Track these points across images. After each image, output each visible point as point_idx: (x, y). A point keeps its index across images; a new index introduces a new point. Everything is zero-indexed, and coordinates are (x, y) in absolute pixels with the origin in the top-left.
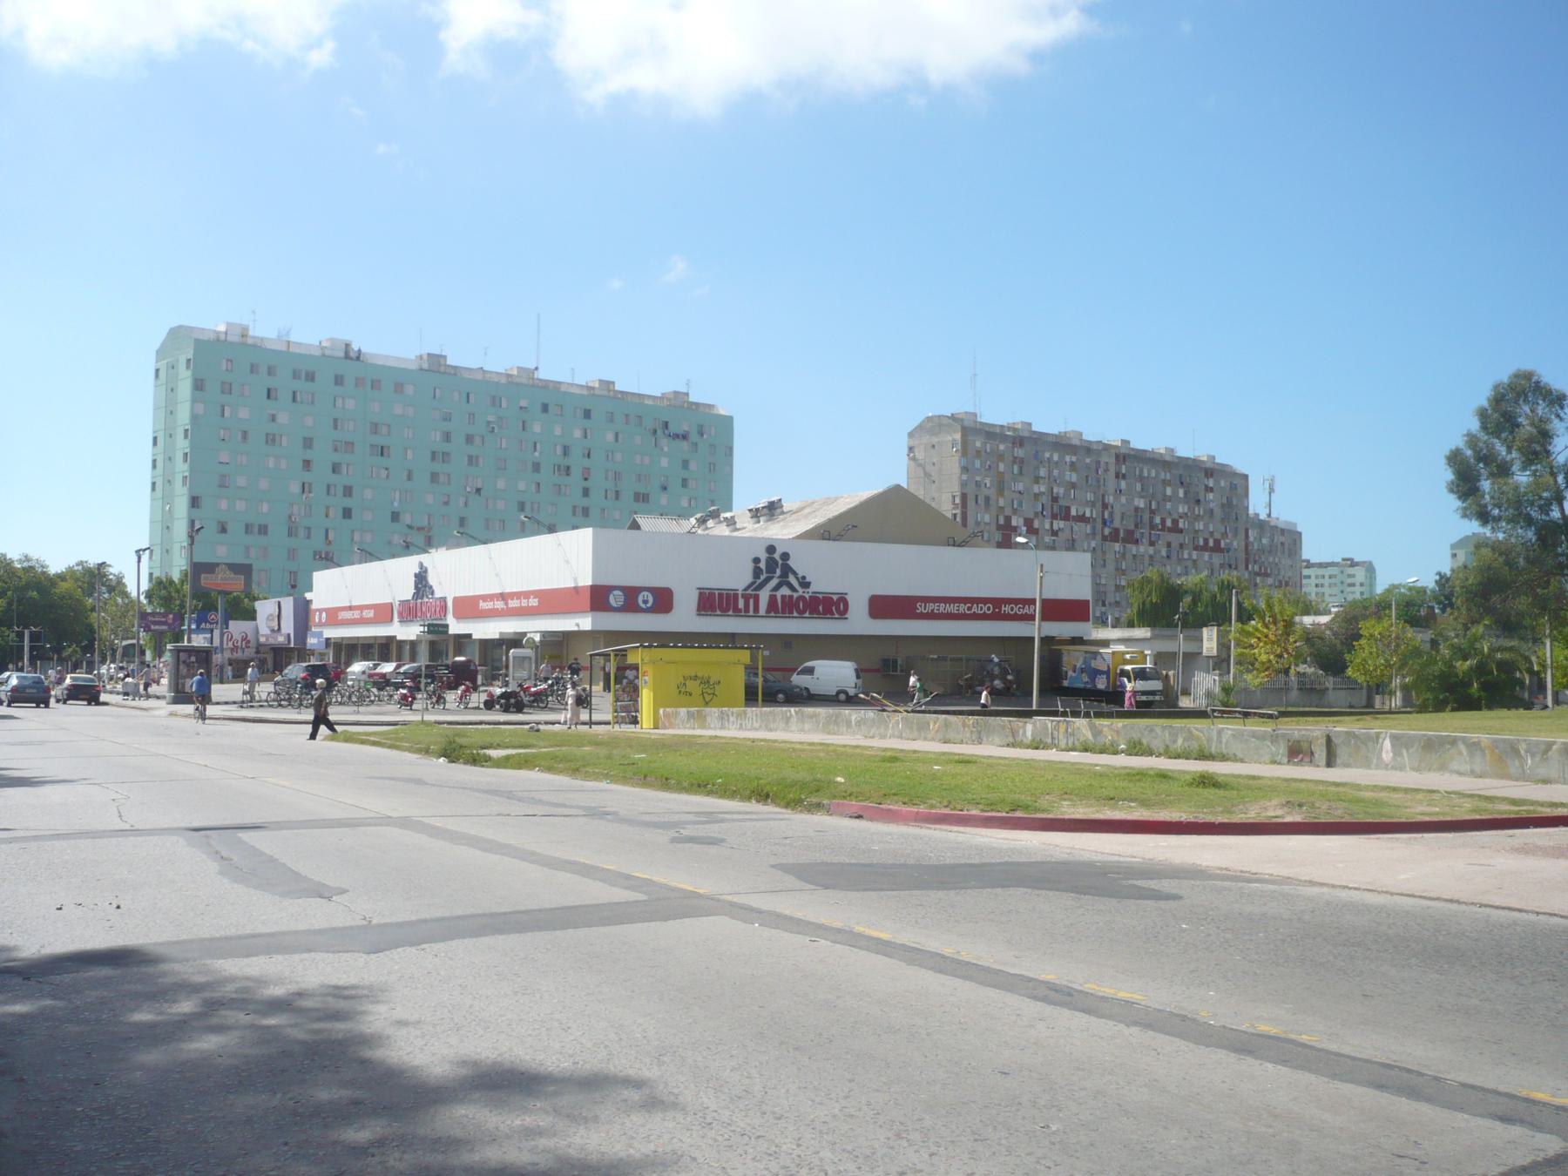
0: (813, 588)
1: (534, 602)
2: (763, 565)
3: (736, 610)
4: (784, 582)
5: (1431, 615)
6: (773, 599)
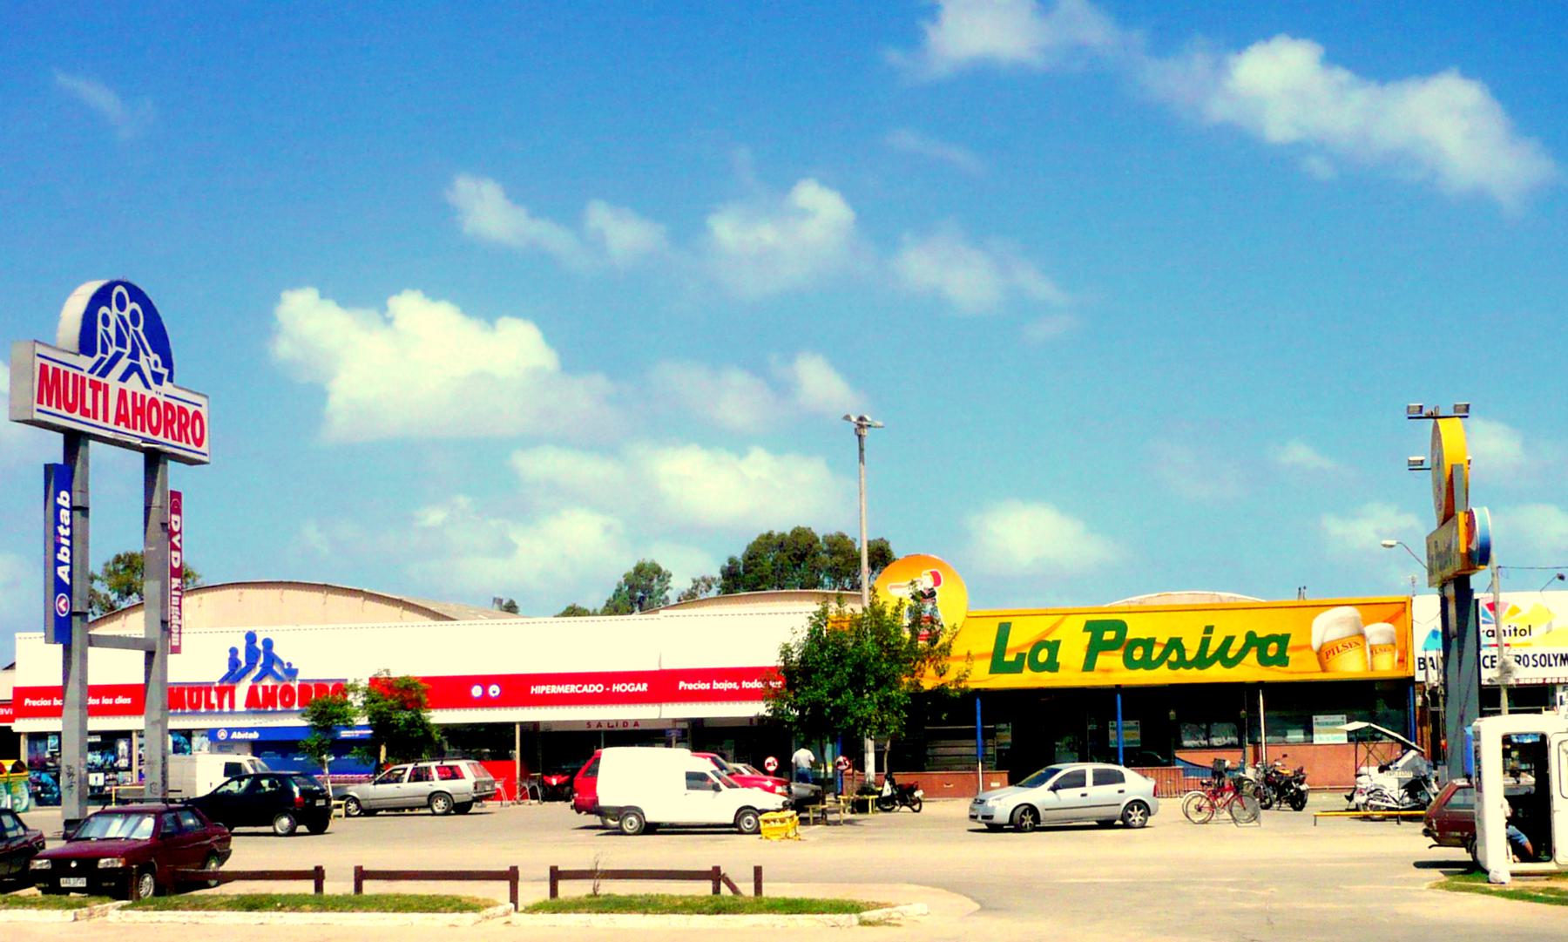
0: (301, 676)
1: (644, 687)
2: (242, 657)
3: (209, 706)
4: (267, 671)
5: (1501, 668)
6: (253, 690)
